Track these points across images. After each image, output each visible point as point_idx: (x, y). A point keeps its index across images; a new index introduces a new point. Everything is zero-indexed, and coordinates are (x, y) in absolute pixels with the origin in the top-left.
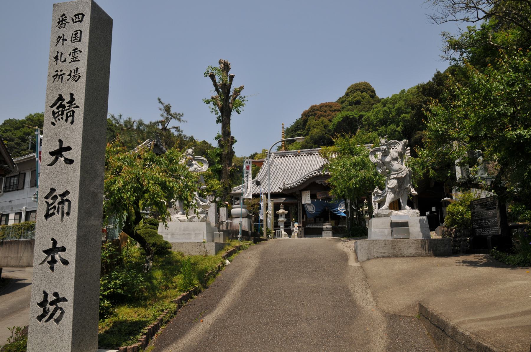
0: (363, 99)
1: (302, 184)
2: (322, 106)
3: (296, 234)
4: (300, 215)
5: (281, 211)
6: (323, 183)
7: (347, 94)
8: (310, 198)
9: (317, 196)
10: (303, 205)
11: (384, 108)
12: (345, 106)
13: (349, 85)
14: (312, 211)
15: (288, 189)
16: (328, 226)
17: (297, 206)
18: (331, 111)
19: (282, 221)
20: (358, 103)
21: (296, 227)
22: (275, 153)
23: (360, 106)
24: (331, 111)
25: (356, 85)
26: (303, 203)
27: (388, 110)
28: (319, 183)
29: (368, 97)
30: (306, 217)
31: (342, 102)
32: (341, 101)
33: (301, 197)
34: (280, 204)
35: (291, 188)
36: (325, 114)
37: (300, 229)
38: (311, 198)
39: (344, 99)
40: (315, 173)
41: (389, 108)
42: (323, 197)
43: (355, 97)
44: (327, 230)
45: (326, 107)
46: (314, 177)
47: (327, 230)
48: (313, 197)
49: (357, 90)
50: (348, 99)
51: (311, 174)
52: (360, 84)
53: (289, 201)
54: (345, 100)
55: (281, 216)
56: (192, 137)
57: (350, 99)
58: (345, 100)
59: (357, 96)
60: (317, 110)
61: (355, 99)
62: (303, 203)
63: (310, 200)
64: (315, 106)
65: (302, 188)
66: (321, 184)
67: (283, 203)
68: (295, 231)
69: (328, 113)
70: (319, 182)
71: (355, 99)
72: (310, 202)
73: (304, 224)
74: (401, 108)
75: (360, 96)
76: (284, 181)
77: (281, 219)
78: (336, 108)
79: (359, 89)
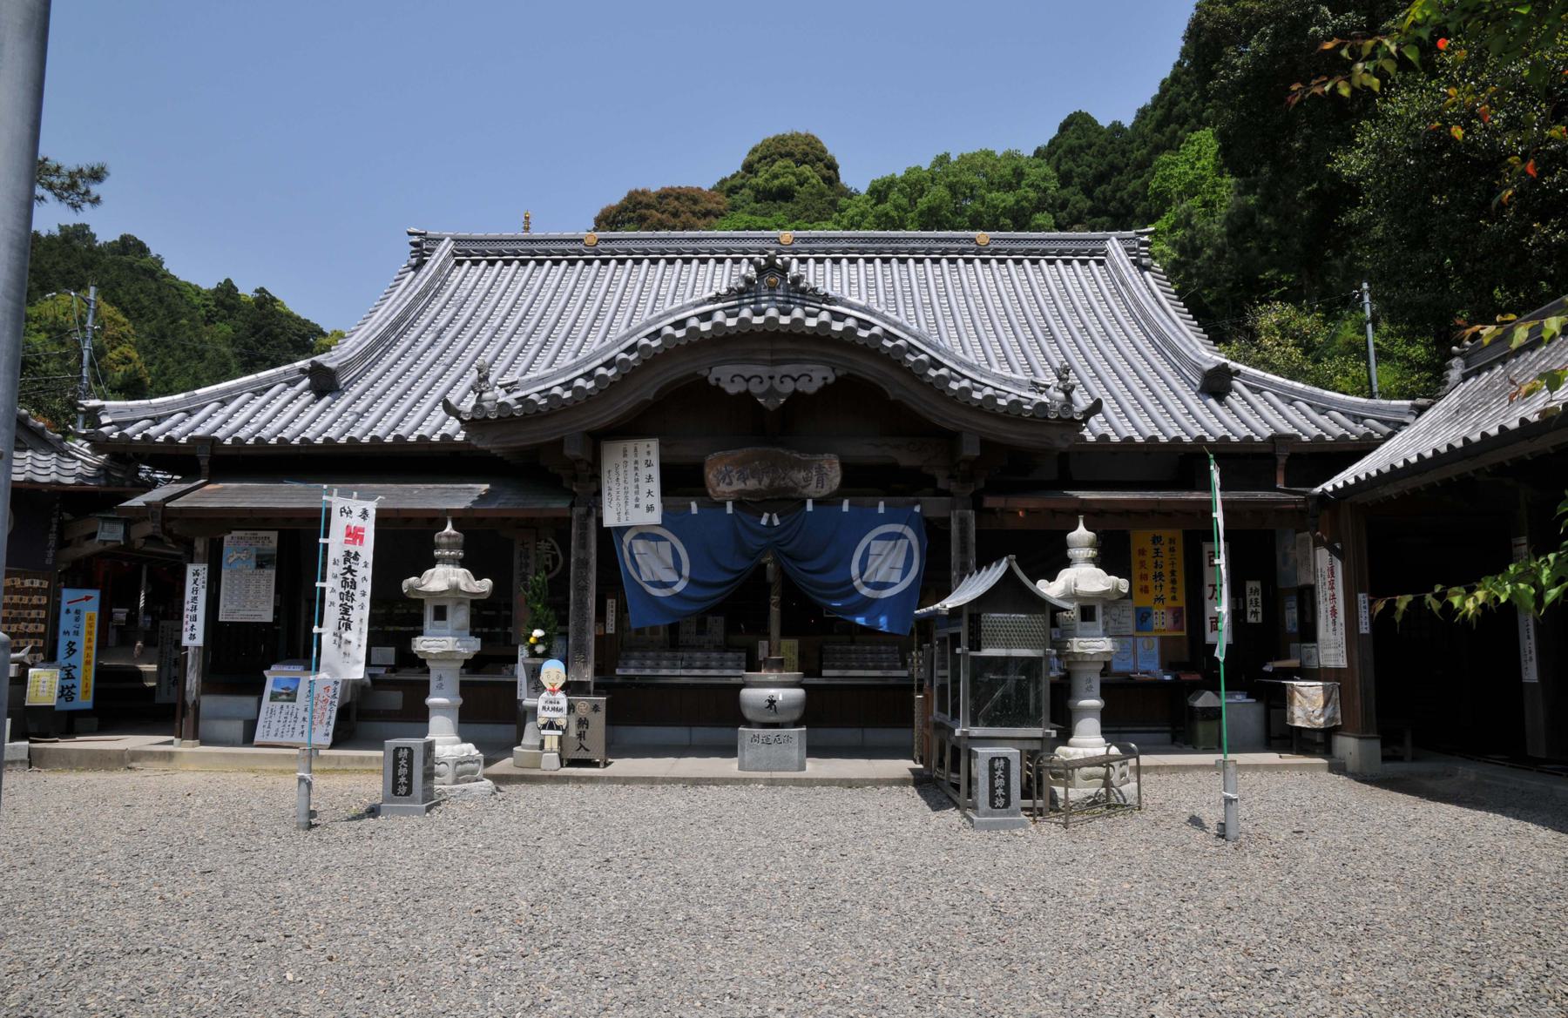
0: (801, 185)
1: (606, 390)
2: (664, 195)
3: (552, 738)
4: (582, 605)
5: (442, 578)
6: (755, 388)
7: (749, 168)
8: (655, 486)
9: (711, 476)
10: (609, 539)
11: (880, 207)
12: (739, 202)
13: (756, 140)
14: (669, 576)
15: (505, 419)
16: (780, 694)
17: (564, 540)
18: (694, 213)
19: (446, 657)
20: (785, 194)
21: (550, 690)
22: (457, 240)
23: (790, 205)
24: (694, 213)
25: (781, 140)
26: (610, 520)
27: (894, 214)
28: (732, 389)
29: (815, 180)
30: (622, 610)
31: (733, 191)
32: (729, 188)
33: (596, 477)
34: (435, 520)
35: (531, 414)
36: (673, 221)
37: (584, 703)
38: (665, 492)
39: (738, 182)
40: (706, 317)
41: (897, 207)
42: (752, 484)
43: (776, 176)
44: (773, 719)
45: (677, 198)
46: (696, 343)
47: (773, 719)
48: (679, 481)
49: (781, 156)
50: (754, 181)
51: (679, 324)
52: (792, 137)
53: (512, 503)
54: (743, 186)
55: (440, 614)
56: (228, 281)
57: (760, 181)
58: (743, 186)
59: (784, 173)
60: (648, 206)
61: (776, 182)
62: (610, 520)
63: (656, 500)
64: (644, 193)
65: (605, 416)
66: (747, 396)
67: (460, 519)
68: (544, 716)
69: (683, 218)
70: (729, 377)
71: (776, 182)
72: (655, 517)
73: (608, 654)
74: (940, 207)
75: (794, 174)
76: (487, 357)
77: (441, 643)
78: (710, 206)
79: (790, 155)
